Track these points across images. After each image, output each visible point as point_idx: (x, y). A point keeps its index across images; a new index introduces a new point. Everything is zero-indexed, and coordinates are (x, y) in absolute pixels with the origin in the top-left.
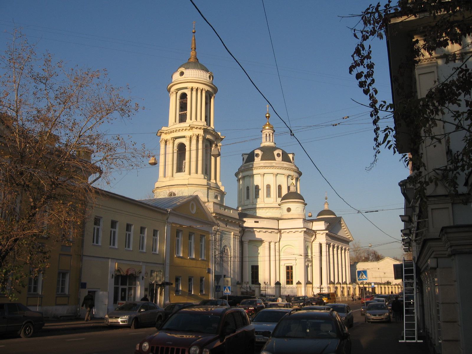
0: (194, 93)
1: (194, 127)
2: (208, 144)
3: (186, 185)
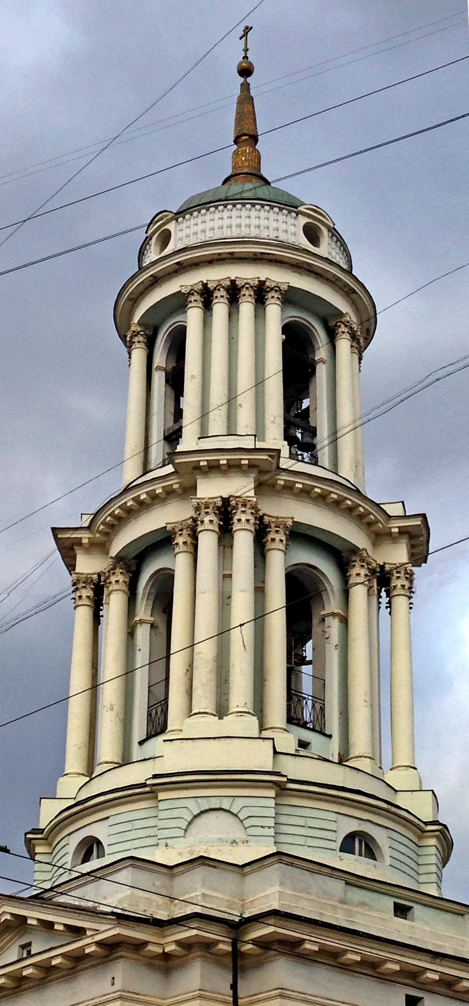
0: (220, 309)
1: (196, 468)
2: (327, 569)
3: (144, 785)
